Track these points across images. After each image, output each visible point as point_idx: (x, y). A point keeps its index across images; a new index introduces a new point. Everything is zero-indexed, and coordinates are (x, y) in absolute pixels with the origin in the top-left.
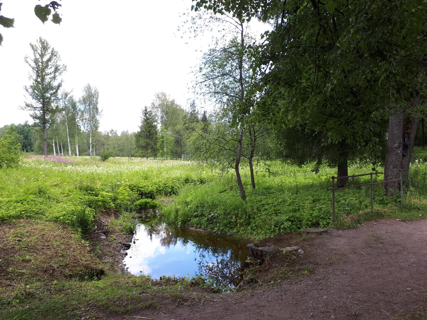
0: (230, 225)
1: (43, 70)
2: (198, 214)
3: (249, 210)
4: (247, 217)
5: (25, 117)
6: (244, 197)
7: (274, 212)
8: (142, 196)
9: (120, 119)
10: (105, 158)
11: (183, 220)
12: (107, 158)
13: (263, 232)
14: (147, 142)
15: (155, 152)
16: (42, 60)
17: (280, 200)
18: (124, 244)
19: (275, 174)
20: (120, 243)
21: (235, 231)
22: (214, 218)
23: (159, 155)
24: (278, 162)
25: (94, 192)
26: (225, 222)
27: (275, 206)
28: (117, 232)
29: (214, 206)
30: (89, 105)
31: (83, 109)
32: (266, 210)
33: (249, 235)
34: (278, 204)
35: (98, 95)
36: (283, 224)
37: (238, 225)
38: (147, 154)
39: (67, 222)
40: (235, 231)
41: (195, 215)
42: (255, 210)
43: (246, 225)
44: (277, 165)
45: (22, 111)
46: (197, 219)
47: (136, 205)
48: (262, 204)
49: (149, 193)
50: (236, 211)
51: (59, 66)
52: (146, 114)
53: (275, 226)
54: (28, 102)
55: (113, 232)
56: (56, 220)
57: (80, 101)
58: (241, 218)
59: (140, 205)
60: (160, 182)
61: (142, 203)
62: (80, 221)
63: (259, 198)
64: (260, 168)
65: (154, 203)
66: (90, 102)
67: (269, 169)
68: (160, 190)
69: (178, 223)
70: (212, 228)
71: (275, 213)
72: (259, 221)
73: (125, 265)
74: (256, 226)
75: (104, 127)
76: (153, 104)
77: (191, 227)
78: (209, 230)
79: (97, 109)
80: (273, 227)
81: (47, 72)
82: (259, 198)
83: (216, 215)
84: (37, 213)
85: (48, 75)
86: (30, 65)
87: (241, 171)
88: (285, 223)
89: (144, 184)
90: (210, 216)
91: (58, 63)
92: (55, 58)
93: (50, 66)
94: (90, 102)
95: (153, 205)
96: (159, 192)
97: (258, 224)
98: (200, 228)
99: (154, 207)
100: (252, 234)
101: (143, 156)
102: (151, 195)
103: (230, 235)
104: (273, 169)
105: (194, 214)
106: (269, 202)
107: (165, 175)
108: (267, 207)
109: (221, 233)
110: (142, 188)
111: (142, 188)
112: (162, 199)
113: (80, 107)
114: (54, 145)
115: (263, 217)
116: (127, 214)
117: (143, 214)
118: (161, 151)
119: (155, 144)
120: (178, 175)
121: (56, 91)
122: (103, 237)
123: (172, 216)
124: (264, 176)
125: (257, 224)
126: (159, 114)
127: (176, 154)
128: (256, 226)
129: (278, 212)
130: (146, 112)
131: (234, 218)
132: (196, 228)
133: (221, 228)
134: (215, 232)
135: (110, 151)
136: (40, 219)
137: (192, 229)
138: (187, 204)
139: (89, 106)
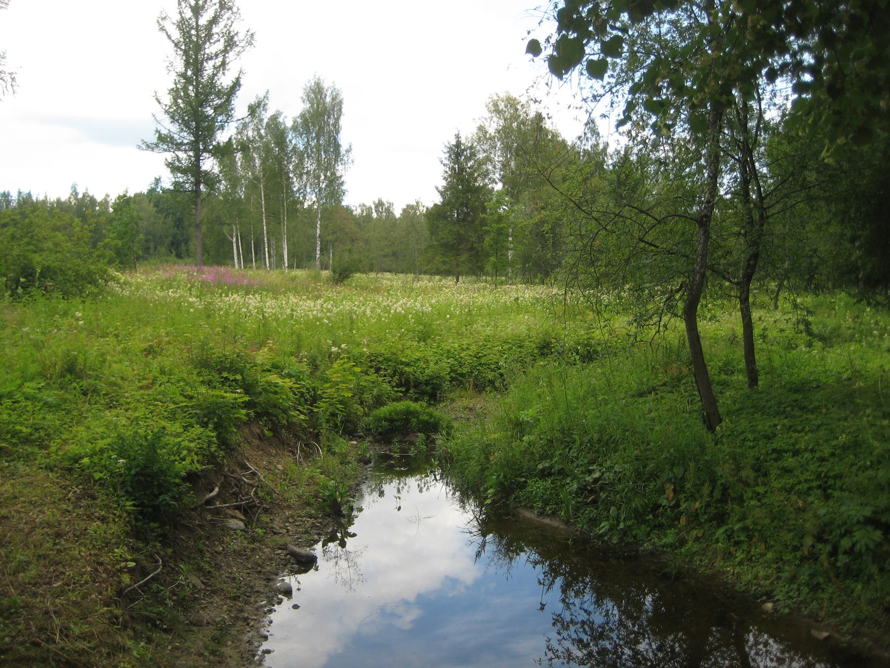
0: (652, 516)
1: (198, 48)
2: (551, 468)
3: (724, 471)
4: (717, 494)
5: (129, 169)
6: (711, 420)
7: (815, 484)
8: (407, 391)
9: (392, 171)
10: (342, 275)
11: (501, 484)
12: (347, 277)
13: (770, 555)
14: (460, 231)
15: (477, 262)
16: (197, 23)
17: (843, 438)
18: (293, 554)
19: (826, 340)
20: (284, 547)
21: (670, 538)
22: (599, 486)
23: (488, 268)
24: (841, 298)
25: (239, 377)
26: (637, 503)
27: (823, 459)
28: (289, 507)
29: (603, 446)
30: (318, 137)
31: (302, 148)
32: (787, 471)
33: (719, 563)
34: (833, 455)
35: (340, 110)
36: (848, 533)
37: (683, 520)
38: (458, 265)
39: (97, 476)
40: (670, 538)
41: (543, 470)
42: (747, 473)
43: (710, 520)
44: (838, 310)
45: (149, 152)
46: (548, 483)
47: (379, 420)
48: (774, 450)
49: (427, 383)
50: (678, 471)
51: (236, 34)
52: (458, 155)
53: (819, 538)
54: (164, 132)
55: (274, 506)
56: (70, 467)
57: (295, 128)
58: (692, 498)
59: (391, 420)
60: (463, 350)
61: (397, 414)
62: (137, 474)
63: (764, 425)
64: (775, 318)
65: (431, 416)
66: (321, 129)
67: (807, 324)
68: (462, 375)
69: (486, 490)
70: (594, 522)
71: (819, 487)
72: (757, 513)
73: (266, 638)
74: (745, 529)
75: (357, 196)
76: (481, 128)
77: (525, 507)
78: (581, 526)
79: (337, 146)
80: (809, 541)
81: (207, 51)
82: (764, 425)
83: (609, 476)
84: (27, 440)
85: (211, 59)
86: (169, 37)
87: (704, 327)
88: (858, 535)
89: (418, 355)
90: (589, 479)
91: (235, 28)
92: (229, 14)
93: (216, 37)
94: (321, 129)
95: (426, 423)
96: (458, 379)
97: (755, 523)
98: (554, 514)
99: (431, 427)
100: (728, 556)
101: (447, 273)
102: (430, 390)
103: (652, 554)
104: (820, 322)
105: (540, 467)
106: (802, 445)
107: (483, 328)
108: (790, 461)
109: (621, 540)
110: (407, 365)
111: (407, 365)
112: (466, 402)
113: (296, 142)
114: (234, 239)
115: (776, 499)
116: (344, 445)
117: (396, 446)
118: (492, 259)
119: (481, 239)
120: (522, 330)
121: (228, 101)
122: (236, 524)
123: (473, 466)
124: (790, 346)
125: (749, 522)
126: (498, 157)
127: (537, 269)
128: (745, 529)
129: (831, 482)
130: (457, 152)
131: (669, 492)
132: (541, 514)
133: (622, 526)
134: (602, 536)
135: (356, 256)
136: (28, 458)
137: (528, 514)
138: (520, 427)
139: (318, 141)
